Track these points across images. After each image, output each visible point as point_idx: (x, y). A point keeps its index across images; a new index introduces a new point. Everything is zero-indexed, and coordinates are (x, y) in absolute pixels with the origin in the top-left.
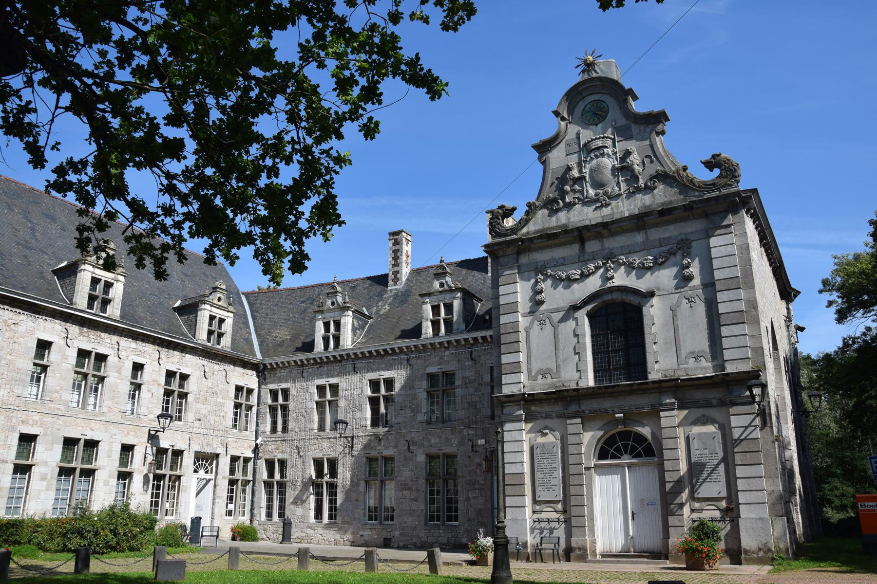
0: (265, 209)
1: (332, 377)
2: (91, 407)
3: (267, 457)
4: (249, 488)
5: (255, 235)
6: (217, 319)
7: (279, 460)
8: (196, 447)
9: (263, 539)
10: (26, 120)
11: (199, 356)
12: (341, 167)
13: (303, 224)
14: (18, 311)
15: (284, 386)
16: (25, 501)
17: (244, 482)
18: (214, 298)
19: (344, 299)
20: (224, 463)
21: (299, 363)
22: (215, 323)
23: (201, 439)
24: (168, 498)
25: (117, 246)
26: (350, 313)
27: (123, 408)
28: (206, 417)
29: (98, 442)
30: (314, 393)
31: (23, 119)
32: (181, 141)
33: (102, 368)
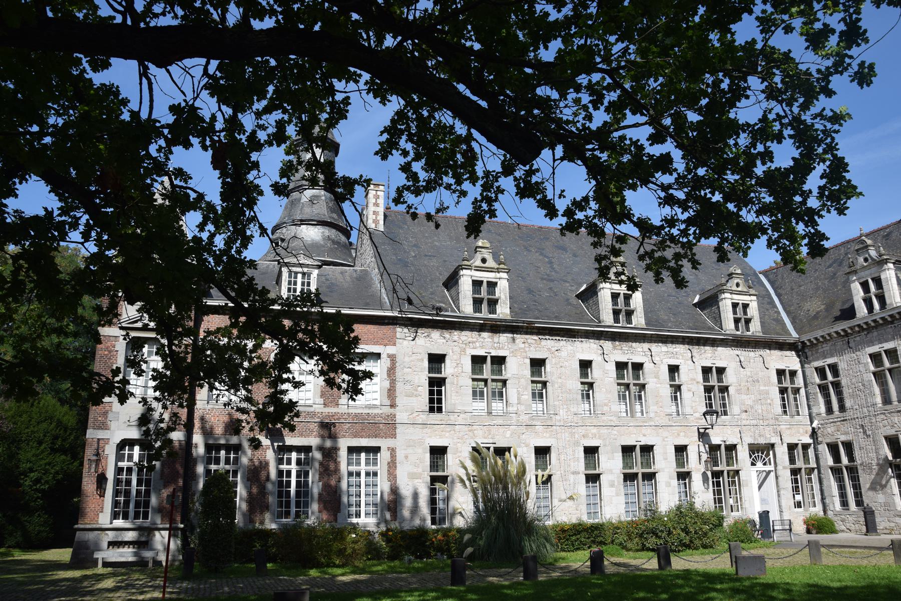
0: (770, 196)
1: (886, 341)
2: (639, 415)
3: (829, 441)
4: (814, 476)
5: (765, 224)
6: (740, 305)
7: (843, 443)
8: (748, 440)
9: (843, 531)
10: (533, 181)
11: (731, 346)
12: (841, 125)
13: (813, 203)
14: (557, 338)
15: (830, 361)
16: (601, 507)
17: (808, 470)
18: (732, 285)
19: (878, 251)
20: (782, 452)
21: (842, 333)
22: (739, 310)
23: (752, 430)
24: (730, 494)
25: (636, 269)
26: (891, 266)
27: (669, 411)
28: (752, 407)
29: (652, 446)
30: (868, 363)
31: (530, 181)
32: (668, 154)
33: (641, 376)
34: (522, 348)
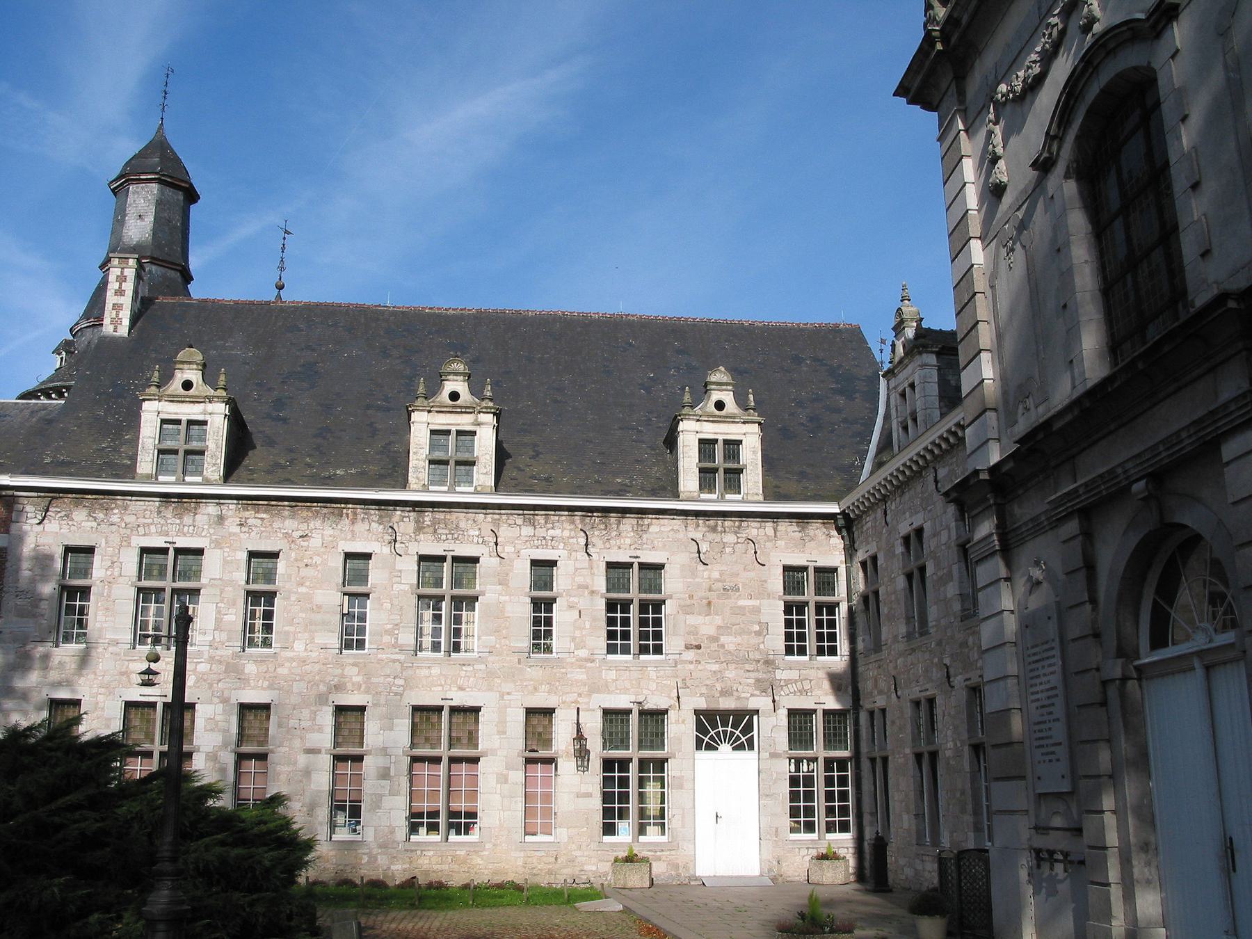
34: (234, 534)
